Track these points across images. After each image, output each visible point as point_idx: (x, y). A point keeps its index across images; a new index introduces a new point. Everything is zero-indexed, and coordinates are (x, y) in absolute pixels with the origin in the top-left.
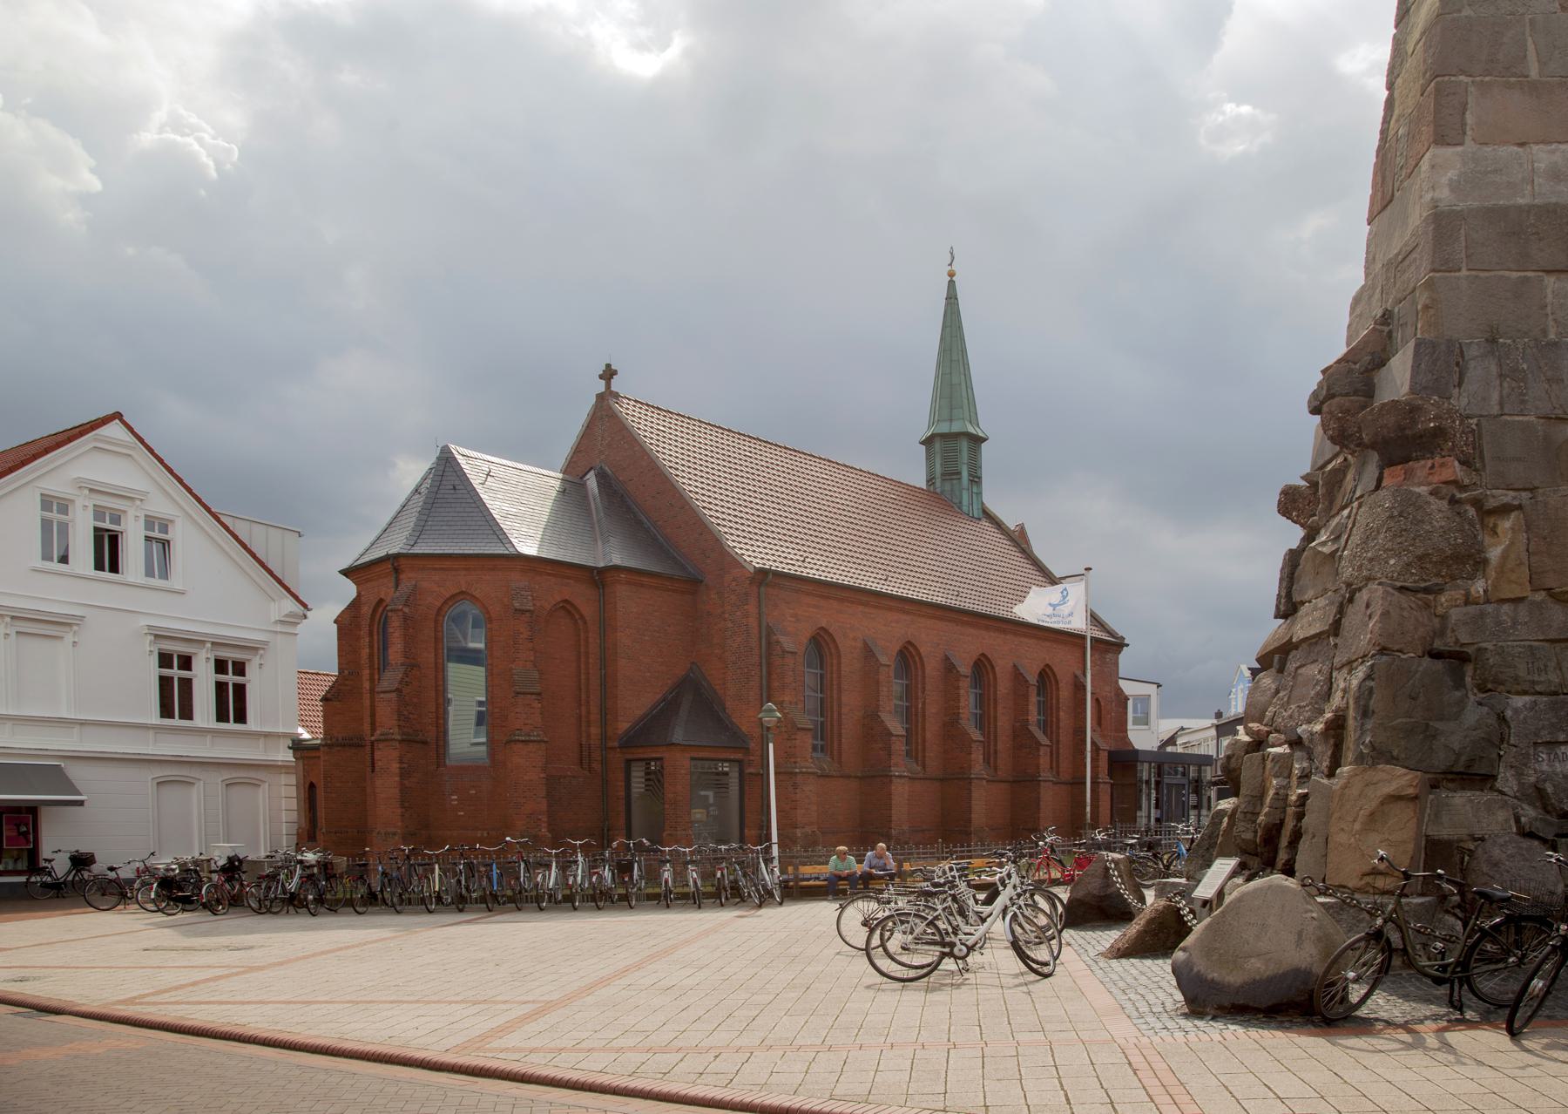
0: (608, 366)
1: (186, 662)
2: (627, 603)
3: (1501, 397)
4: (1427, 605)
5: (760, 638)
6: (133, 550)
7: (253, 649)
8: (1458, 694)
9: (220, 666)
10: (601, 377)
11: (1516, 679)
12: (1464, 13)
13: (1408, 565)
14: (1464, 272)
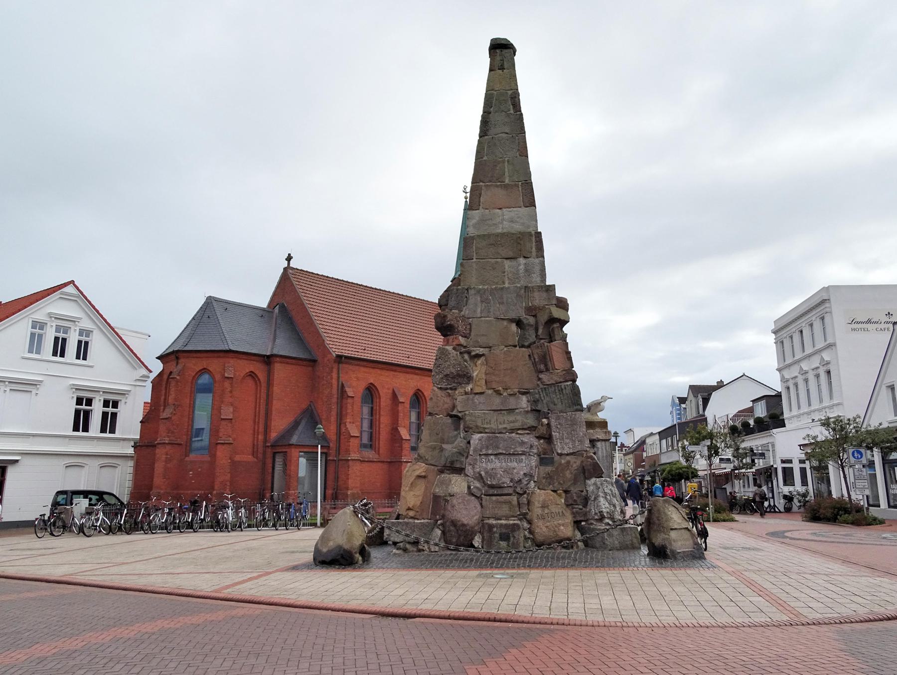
0: (289, 255)
1: (89, 402)
2: (280, 371)
3: (481, 310)
4: (449, 395)
5: (338, 390)
6: (71, 348)
7: (123, 394)
8: (456, 433)
9: (106, 404)
10: (286, 259)
11: (477, 427)
12: (484, 159)
13: (442, 378)
14: (475, 260)
